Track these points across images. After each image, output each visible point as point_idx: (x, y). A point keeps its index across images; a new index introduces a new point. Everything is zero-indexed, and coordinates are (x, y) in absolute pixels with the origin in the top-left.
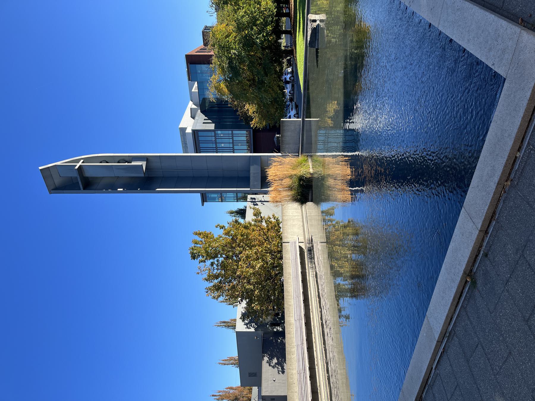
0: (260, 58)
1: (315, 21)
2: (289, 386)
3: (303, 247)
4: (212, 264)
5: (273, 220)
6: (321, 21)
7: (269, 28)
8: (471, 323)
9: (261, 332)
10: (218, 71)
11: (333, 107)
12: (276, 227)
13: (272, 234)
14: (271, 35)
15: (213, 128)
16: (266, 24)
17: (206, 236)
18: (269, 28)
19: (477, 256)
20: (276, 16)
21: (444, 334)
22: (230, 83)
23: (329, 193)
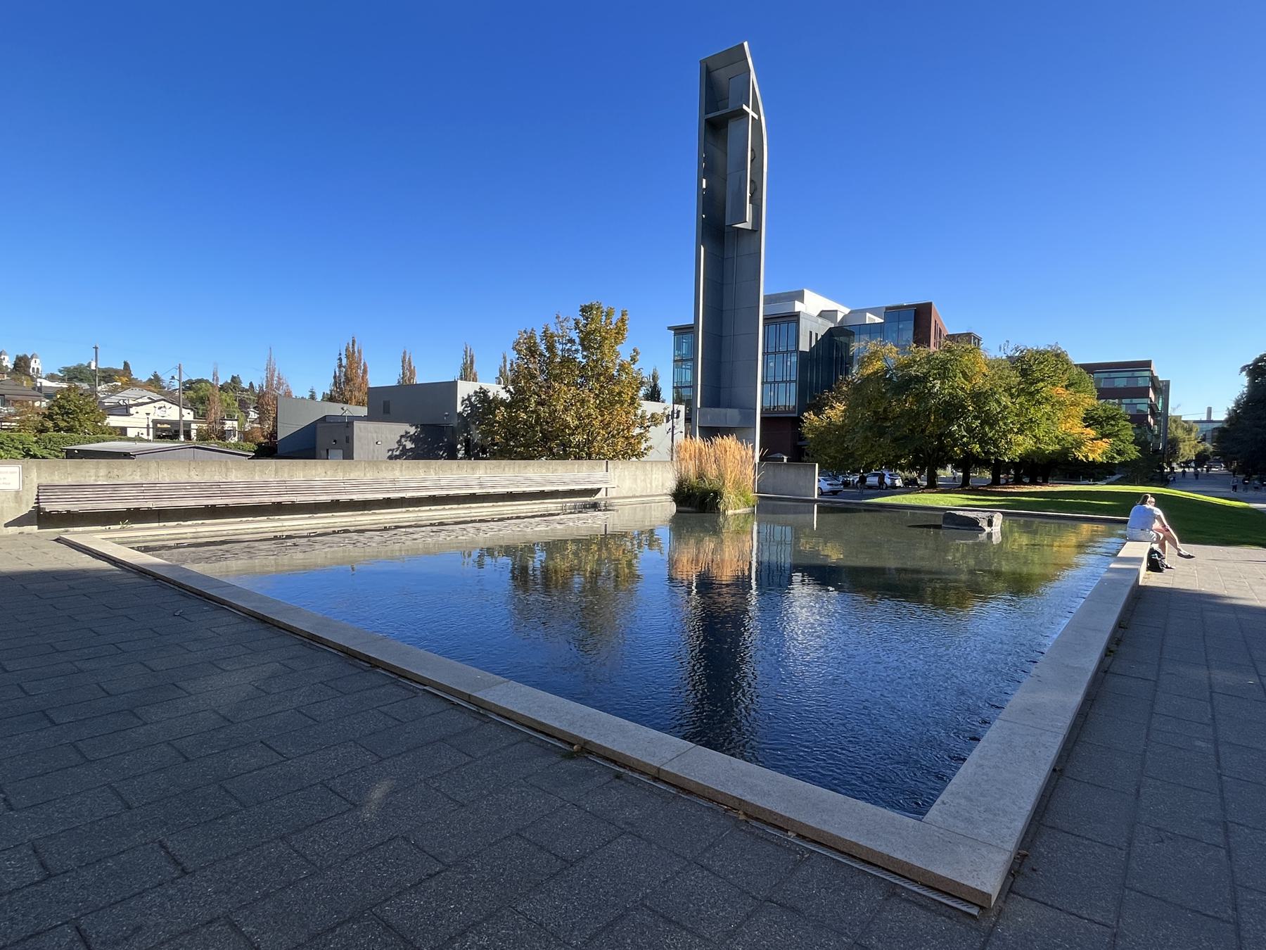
0: (923, 431)
1: (990, 524)
2: (373, 463)
3: (599, 496)
4: (572, 341)
5: (643, 446)
6: (990, 535)
7: (977, 448)
8: (504, 748)
9: (455, 422)
10: (904, 359)
11: (833, 554)
12: (631, 451)
13: (621, 444)
14: (962, 450)
15: (801, 349)
16: (983, 442)
17: (619, 332)
18: (977, 448)
19: (615, 762)
20: (996, 460)
21: (481, 705)
22: (877, 377)
23: (692, 541)
